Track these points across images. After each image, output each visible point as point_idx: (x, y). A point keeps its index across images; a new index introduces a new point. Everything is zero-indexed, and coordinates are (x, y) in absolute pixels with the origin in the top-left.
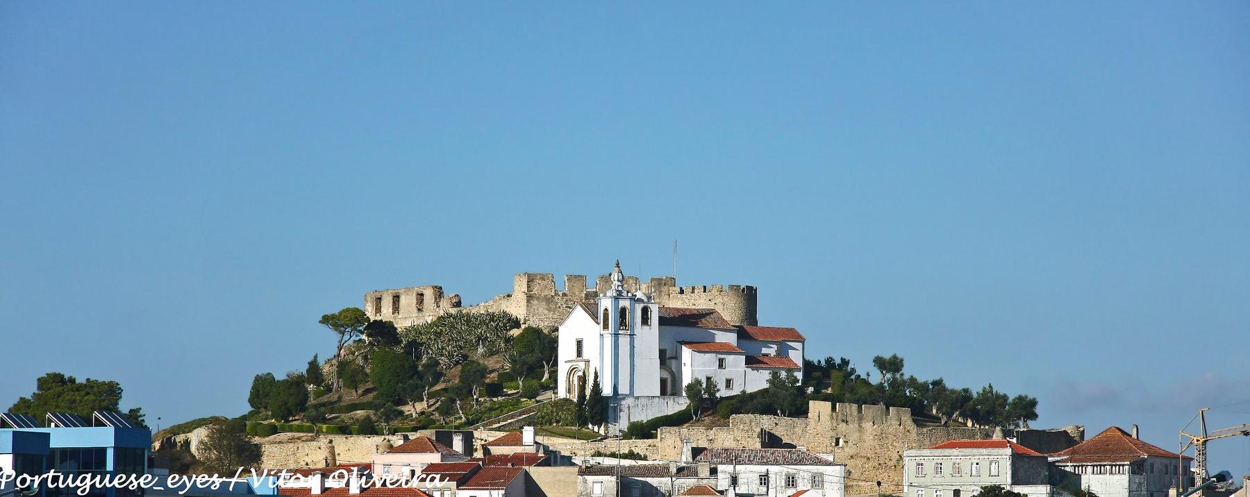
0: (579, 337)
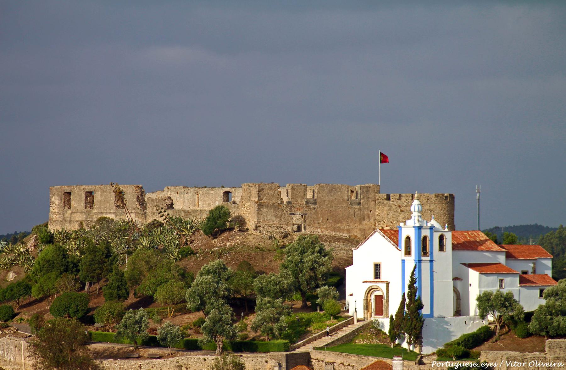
0: (377, 262)
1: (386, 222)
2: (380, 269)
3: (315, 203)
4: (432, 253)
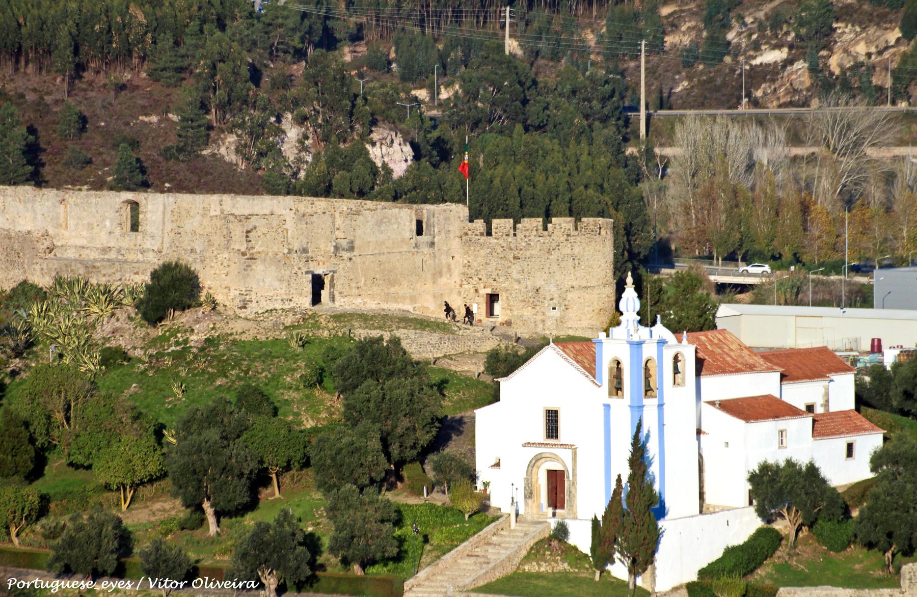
0: (552, 407)
1: (484, 278)
2: (556, 421)
3: (351, 249)
4: (661, 389)
